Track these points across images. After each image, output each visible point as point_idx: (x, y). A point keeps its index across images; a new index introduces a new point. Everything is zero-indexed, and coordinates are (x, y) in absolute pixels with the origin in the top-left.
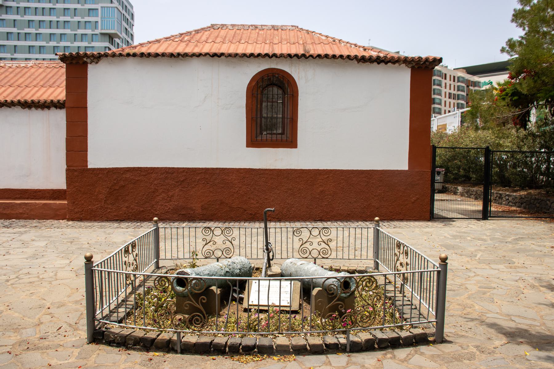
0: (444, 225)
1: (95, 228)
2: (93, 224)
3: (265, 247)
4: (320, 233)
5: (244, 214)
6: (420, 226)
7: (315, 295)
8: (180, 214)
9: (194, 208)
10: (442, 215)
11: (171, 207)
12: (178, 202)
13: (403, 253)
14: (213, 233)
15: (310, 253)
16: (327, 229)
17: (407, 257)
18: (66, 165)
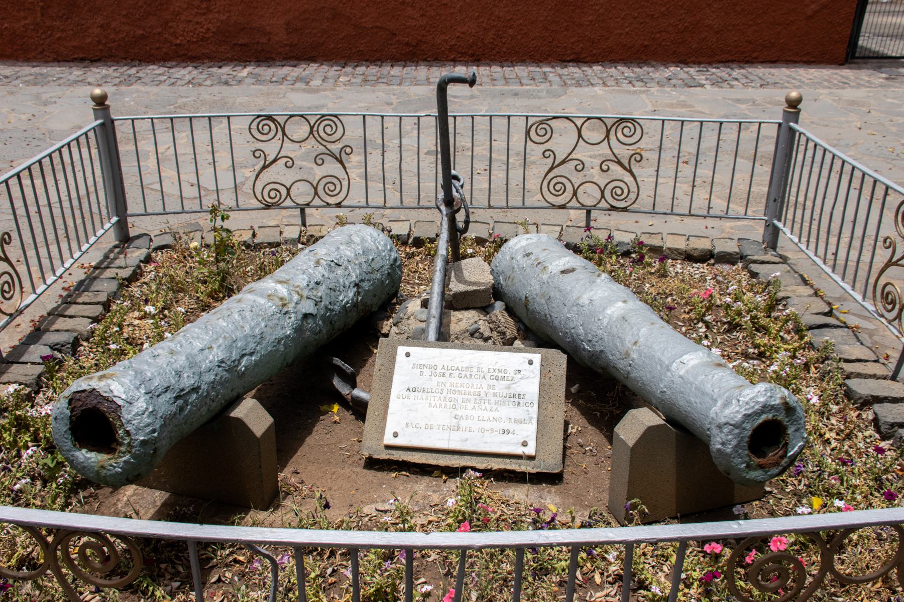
0: (886, 79)
1: (17, 82)
2: (18, 72)
3: (441, 195)
4: (607, 136)
5: (391, 45)
6: (826, 80)
7: (631, 443)
8: (235, 45)
9: (268, 29)
10: (869, 46)
11: (210, 26)
12: (227, 14)
14: (284, 134)
15: (575, 193)
16: (629, 125)
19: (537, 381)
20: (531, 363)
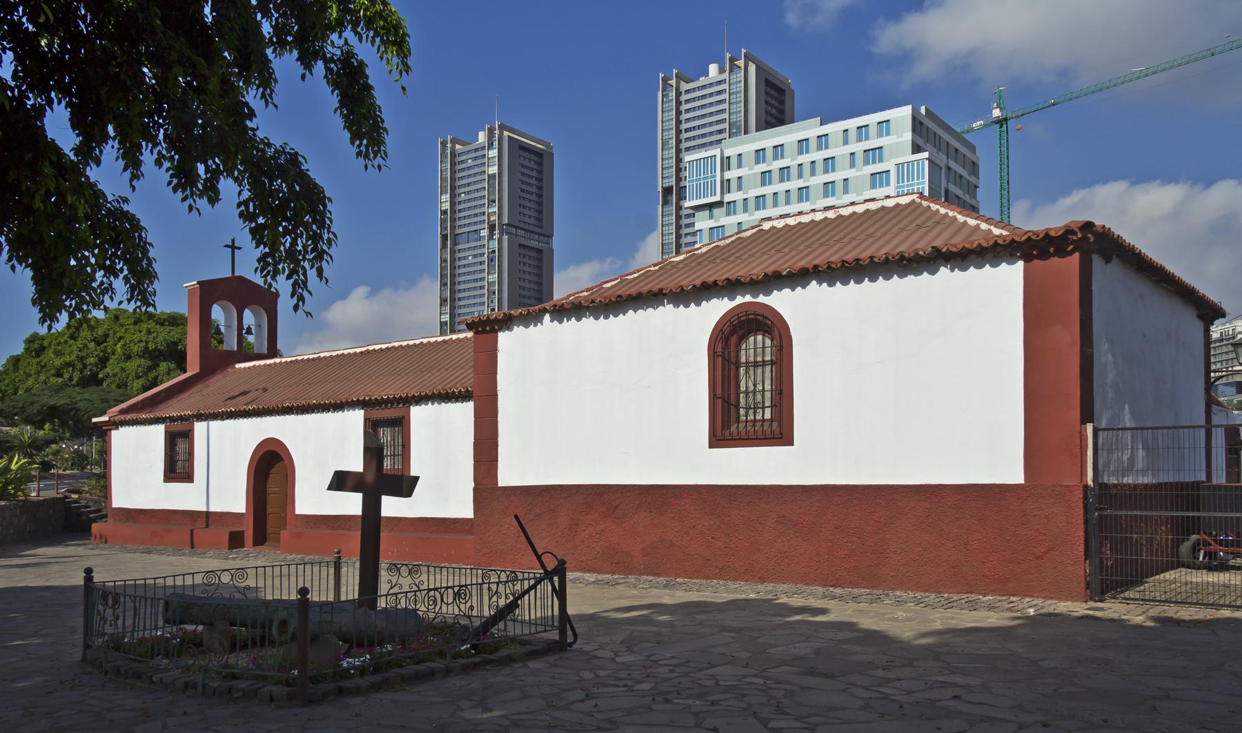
14: (400, 574)
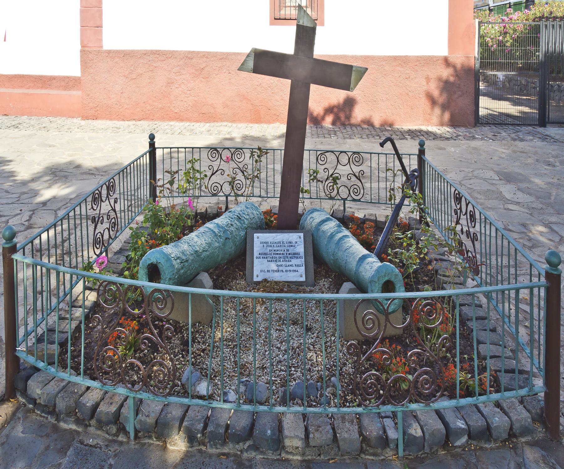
13: (466, 213)
17: (473, 224)
18: (81, 45)
19: (303, 246)
20: (300, 238)
